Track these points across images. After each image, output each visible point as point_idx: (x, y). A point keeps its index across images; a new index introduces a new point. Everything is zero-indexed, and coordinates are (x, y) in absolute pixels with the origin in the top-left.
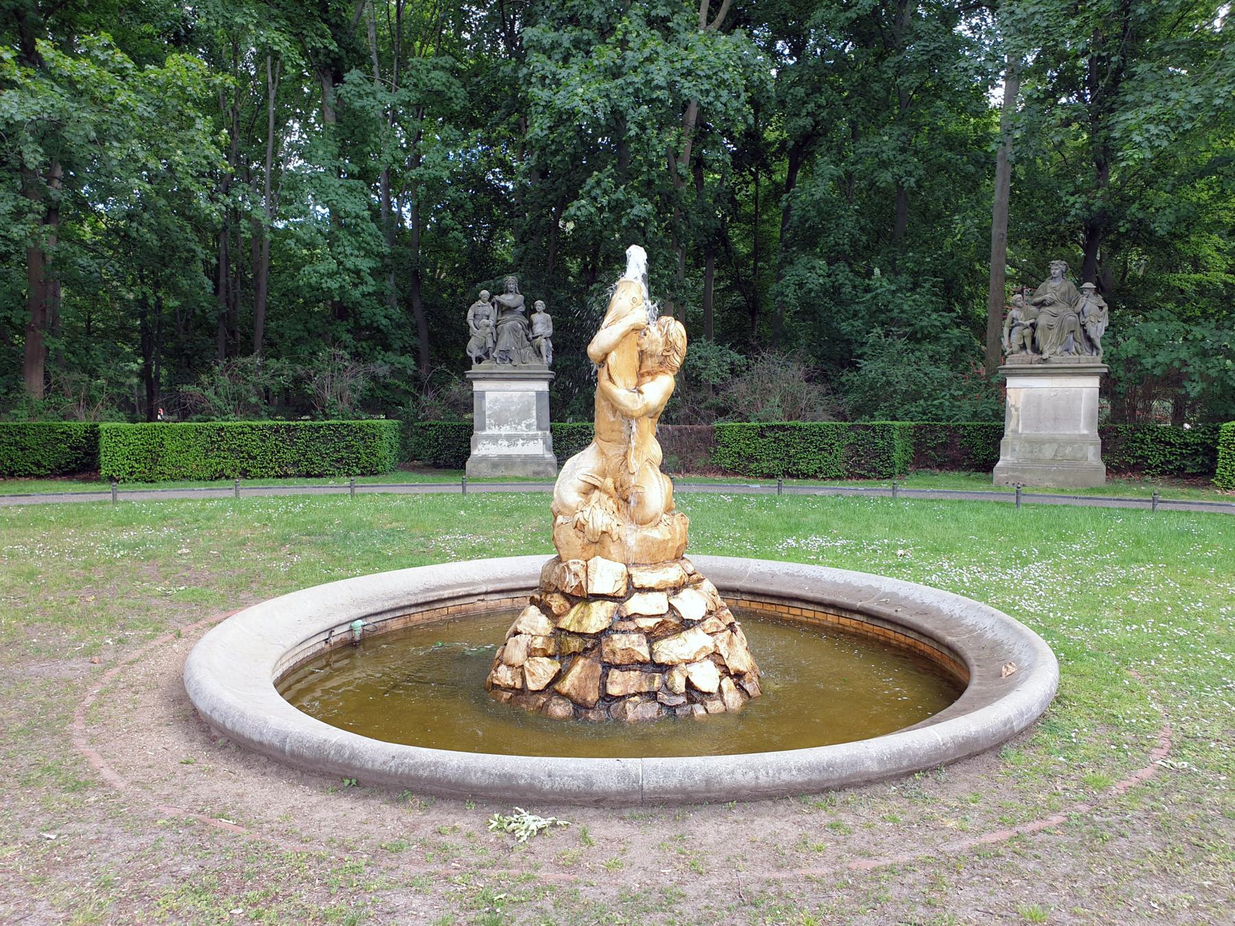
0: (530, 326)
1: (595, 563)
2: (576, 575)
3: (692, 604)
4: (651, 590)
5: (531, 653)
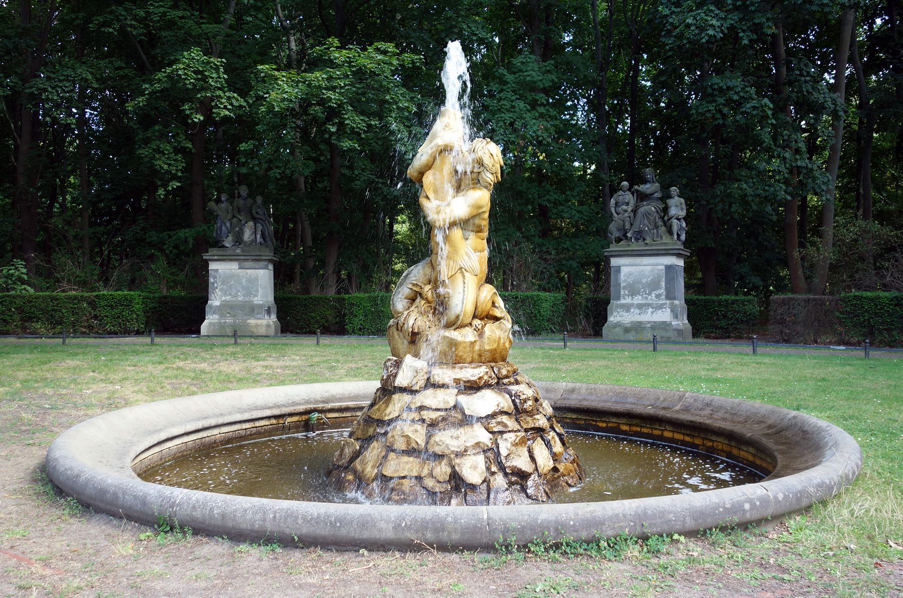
0: (666, 210)
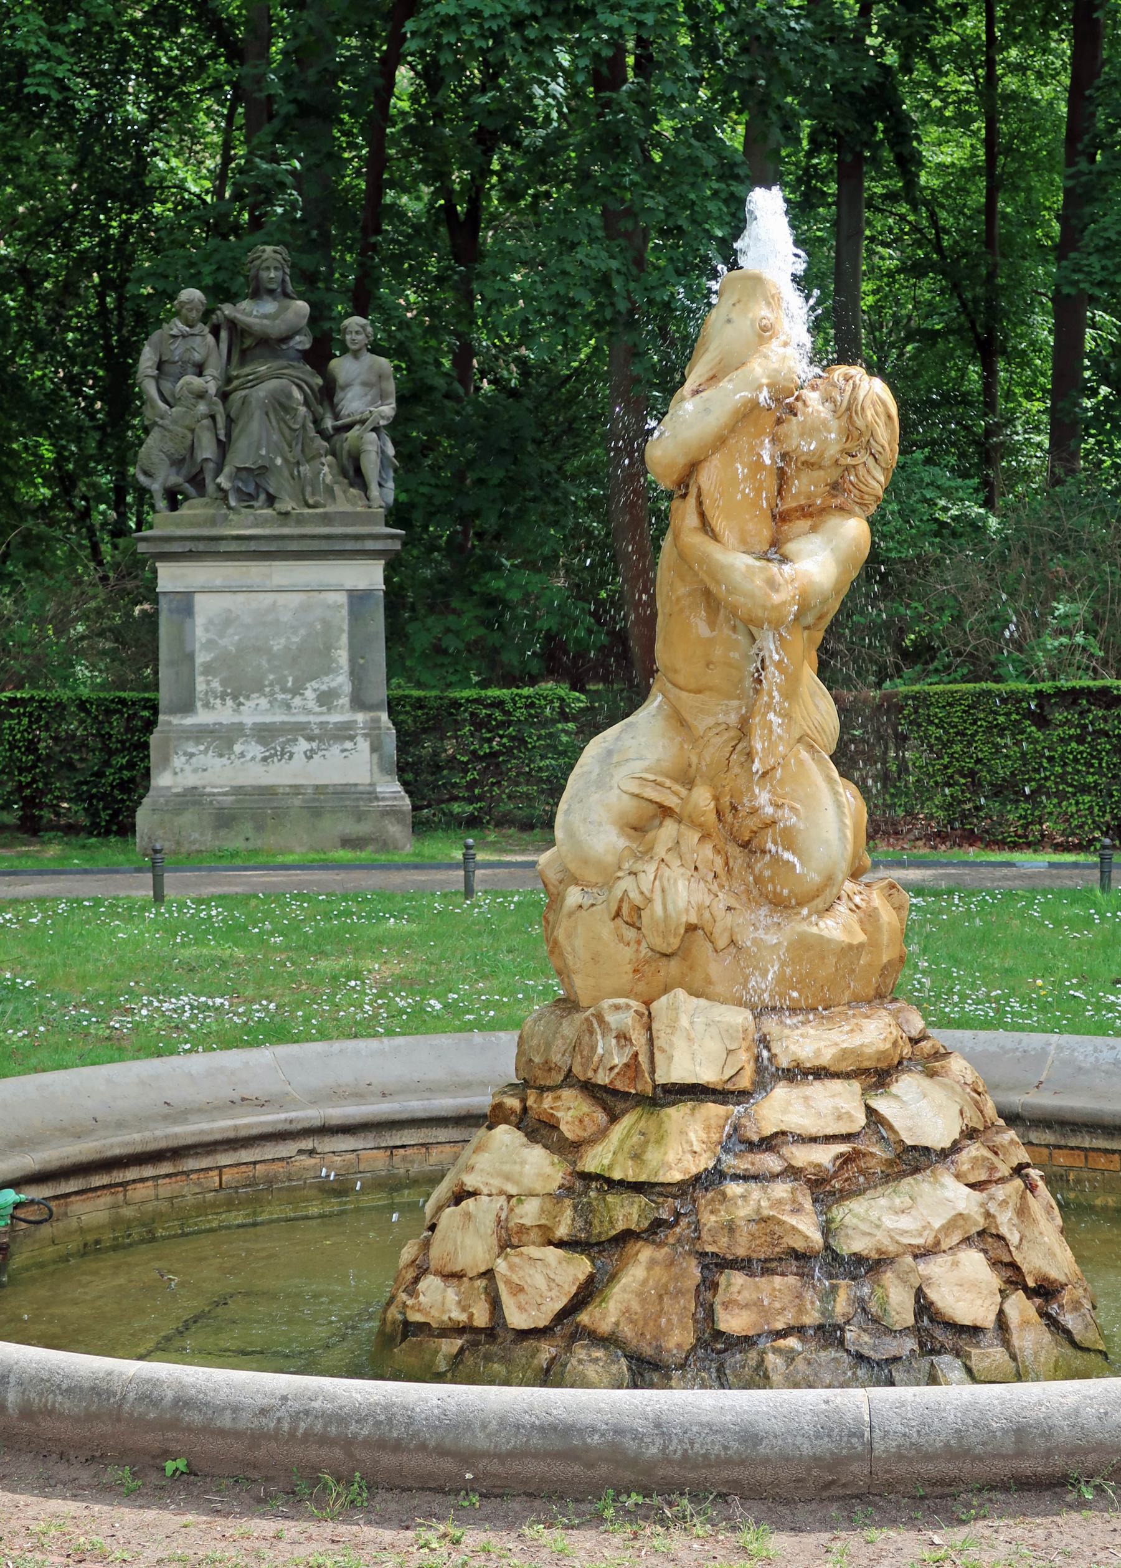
0: (328, 393)
1: (674, 1008)
2: (623, 1037)
3: (922, 1111)
4: (820, 1073)
5: (508, 1240)
